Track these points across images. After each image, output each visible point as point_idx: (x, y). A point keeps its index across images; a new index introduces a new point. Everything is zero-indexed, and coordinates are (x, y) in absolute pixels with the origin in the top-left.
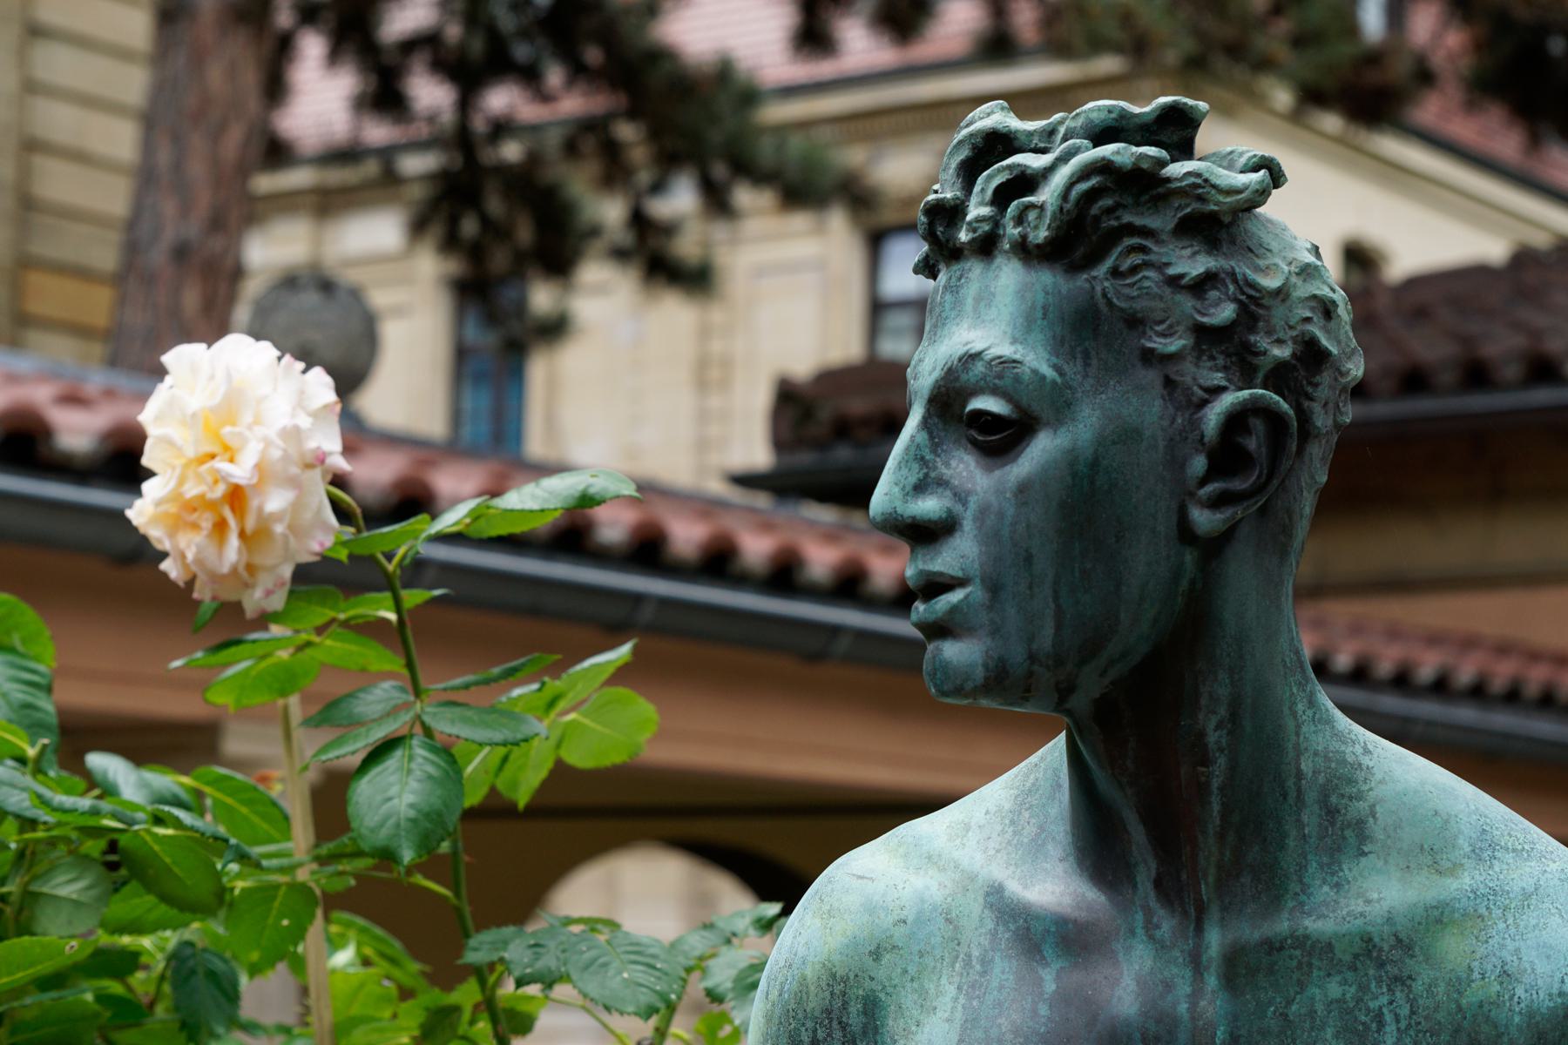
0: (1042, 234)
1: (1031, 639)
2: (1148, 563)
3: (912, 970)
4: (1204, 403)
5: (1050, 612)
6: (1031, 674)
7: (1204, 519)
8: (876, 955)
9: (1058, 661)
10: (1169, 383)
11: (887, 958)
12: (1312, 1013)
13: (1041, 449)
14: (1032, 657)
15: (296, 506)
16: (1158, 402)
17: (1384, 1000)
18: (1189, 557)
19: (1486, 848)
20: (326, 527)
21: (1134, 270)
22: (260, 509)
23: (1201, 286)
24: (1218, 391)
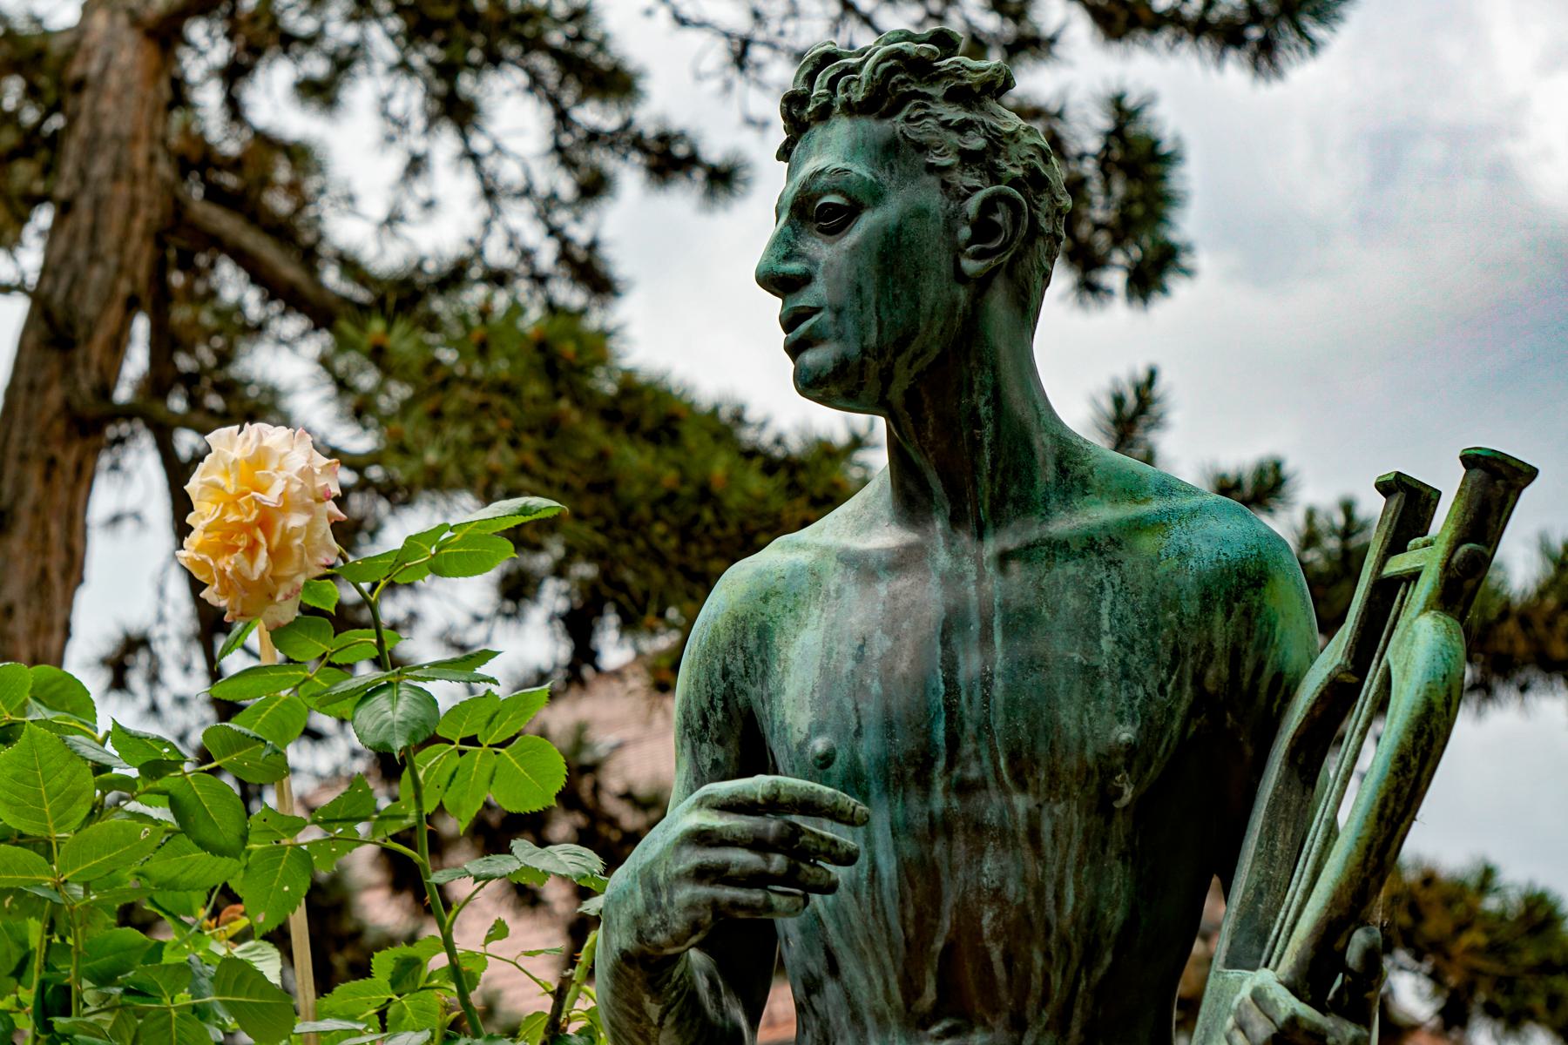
0: (858, 96)
1: (863, 339)
3: (790, 605)
4: (967, 197)
5: (874, 322)
6: (863, 363)
7: (970, 266)
8: (765, 600)
9: (881, 352)
10: (945, 186)
11: (772, 600)
12: (1057, 583)
13: (868, 221)
14: (864, 351)
15: (311, 527)
16: (938, 196)
17: (1104, 574)
20: (330, 548)
21: (919, 118)
22: (284, 527)
23: (963, 127)
24: (976, 189)
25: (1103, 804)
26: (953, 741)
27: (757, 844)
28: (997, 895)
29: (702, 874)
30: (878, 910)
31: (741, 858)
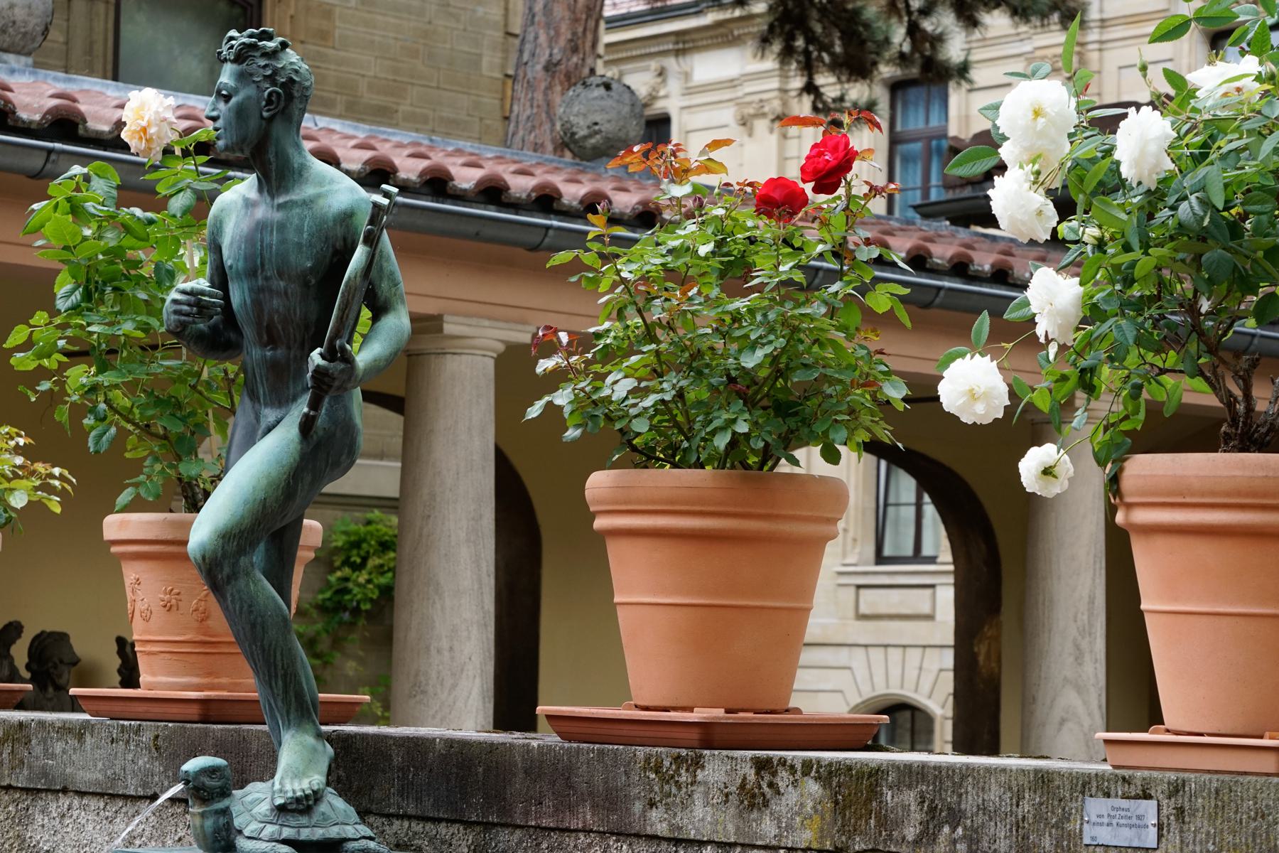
2: (253, 123)
7: (265, 114)
13: (234, 100)
18: (264, 123)
19: (332, 182)
23: (265, 66)
25: (306, 284)
26: (263, 265)
27: (189, 305)
28: (277, 311)
29: (176, 312)
30: (247, 313)
31: (185, 308)
